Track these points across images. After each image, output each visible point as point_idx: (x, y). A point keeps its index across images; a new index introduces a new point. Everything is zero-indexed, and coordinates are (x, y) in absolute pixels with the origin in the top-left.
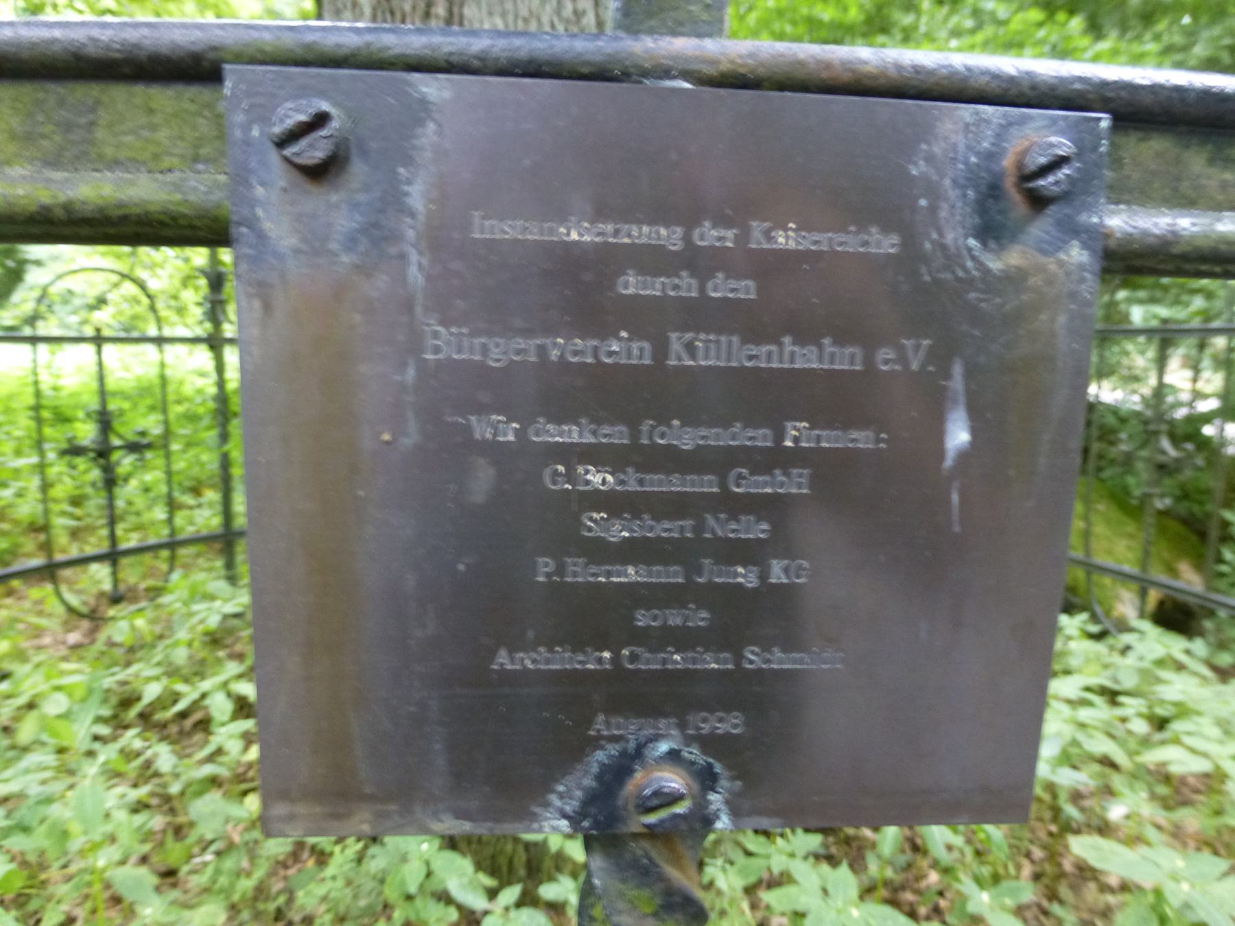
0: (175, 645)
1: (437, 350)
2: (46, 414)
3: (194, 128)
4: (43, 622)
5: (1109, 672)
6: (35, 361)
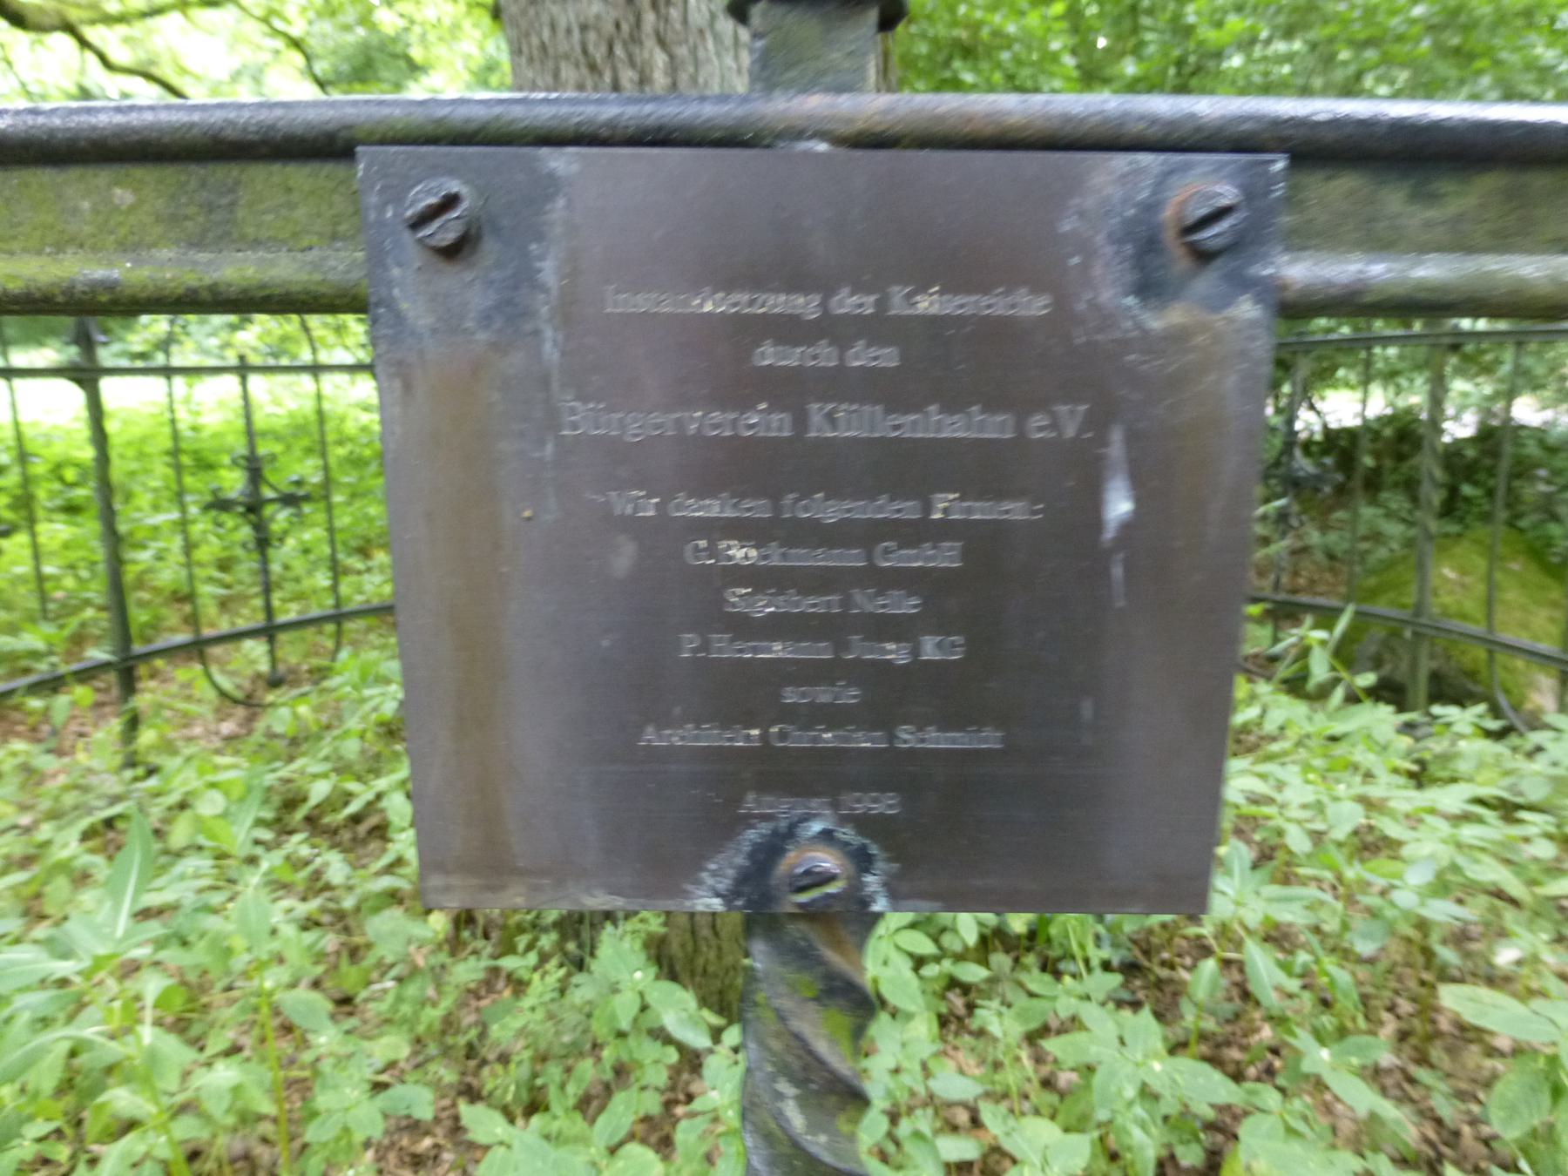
0: (347, 733)
1: (575, 426)
2: (186, 460)
3: (331, 205)
4: (192, 708)
5: (1507, 781)
6: (170, 395)
